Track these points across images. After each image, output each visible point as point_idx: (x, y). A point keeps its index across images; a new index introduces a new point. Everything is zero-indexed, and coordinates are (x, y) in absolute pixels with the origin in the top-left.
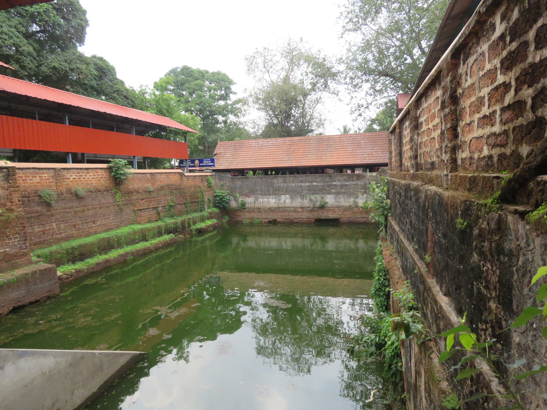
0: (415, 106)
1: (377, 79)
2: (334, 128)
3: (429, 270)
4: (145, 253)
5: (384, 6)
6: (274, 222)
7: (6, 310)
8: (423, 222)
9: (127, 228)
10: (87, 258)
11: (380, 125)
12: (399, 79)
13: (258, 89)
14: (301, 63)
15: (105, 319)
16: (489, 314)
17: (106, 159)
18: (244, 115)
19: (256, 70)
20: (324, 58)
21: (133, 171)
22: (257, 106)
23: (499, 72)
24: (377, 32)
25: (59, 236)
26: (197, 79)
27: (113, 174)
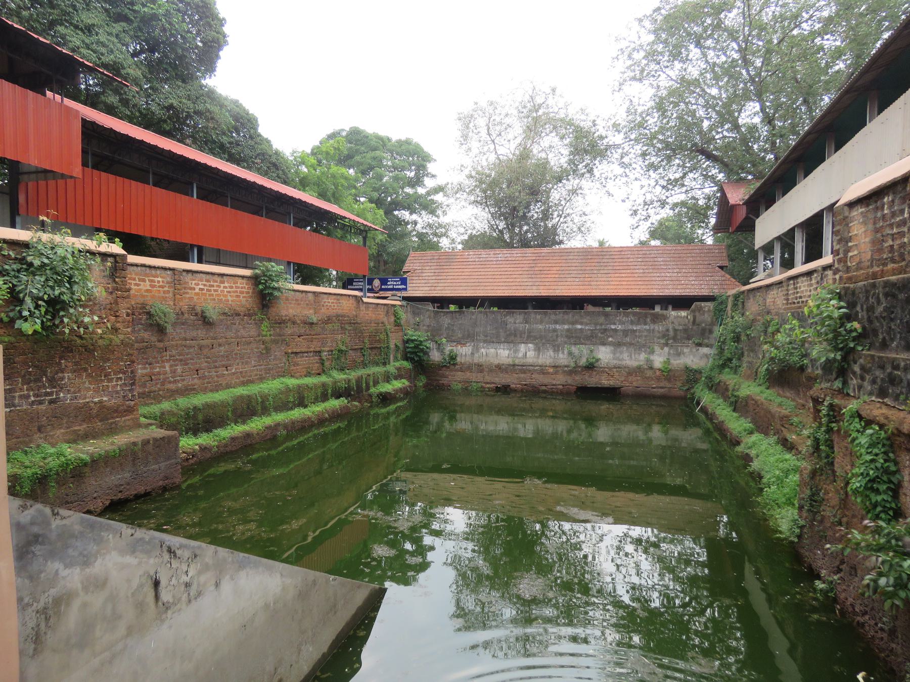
4: (304, 426)
6: (505, 390)
10: (216, 428)
20: (594, 121)
25: (172, 386)
26: (375, 149)
27: (261, 287)
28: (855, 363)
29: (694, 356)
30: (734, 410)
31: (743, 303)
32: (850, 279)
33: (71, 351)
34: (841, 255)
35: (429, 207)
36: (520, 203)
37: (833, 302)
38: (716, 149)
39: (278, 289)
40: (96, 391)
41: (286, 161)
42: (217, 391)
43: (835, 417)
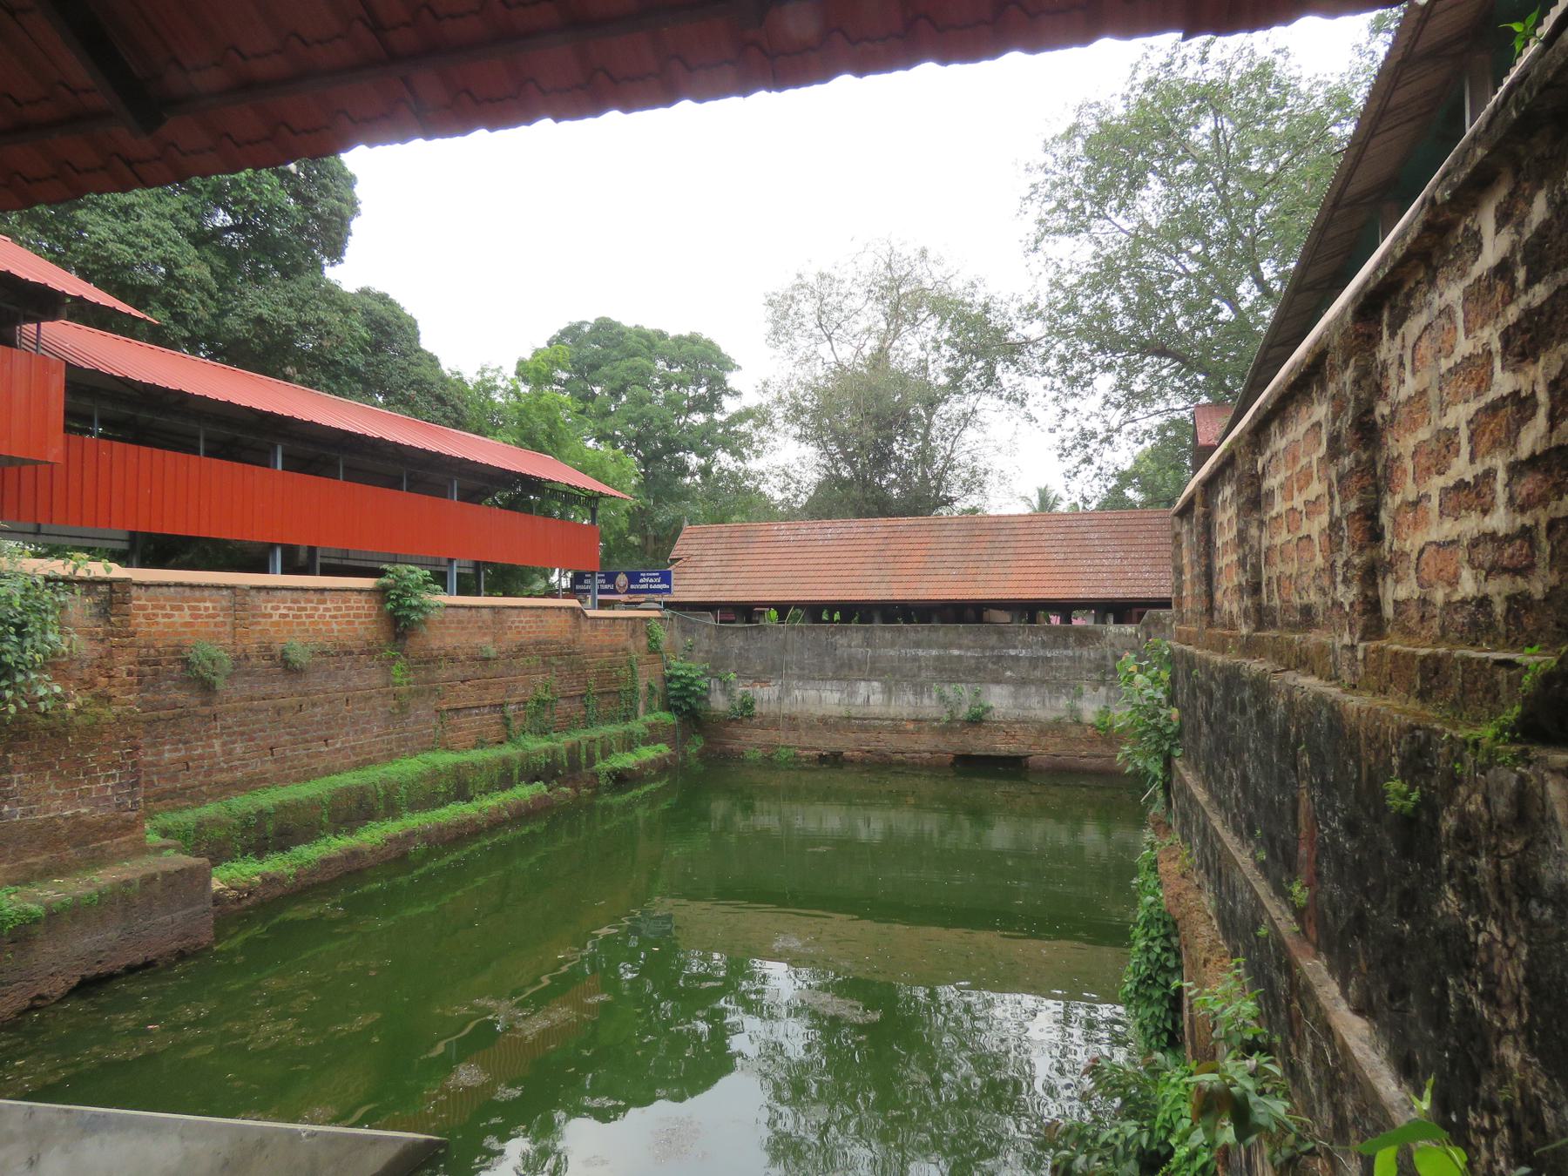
0: (1249, 444)
1: (1136, 361)
2: (1012, 494)
3: (1304, 931)
5: (1154, 170)
6: (834, 760)
7: (60, 986)
8: (1282, 783)
9: (414, 760)
10: (297, 844)
11: (1143, 490)
12: (1199, 365)
13: (800, 383)
14: (921, 316)
15: (332, 1029)
16: (1503, 1081)
17: (375, 565)
18: (758, 454)
19: (798, 332)
20: (986, 305)
21: (444, 599)
22: (796, 430)
23: (1498, 363)
24: (1136, 236)
25: (225, 777)
27: (389, 606)
33: (26, 738)
40: (69, 798)
42: (308, 780)
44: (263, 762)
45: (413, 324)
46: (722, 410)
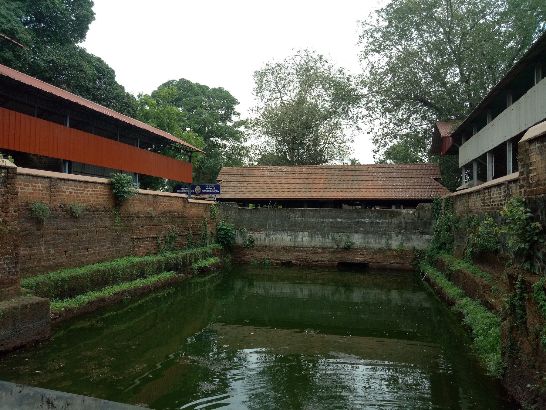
4: (144, 292)
6: (288, 264)
9: (123, 260)
10: (78, 295)
18: (246, 140)
20: (348, 79)
25: (45, 264)
28: (539, 251)
29: (419, 241)
30: (449, 280)
31: (453, 204)
32: (532, 192)
34: (525, 176)
35: (235, 135)
36: (299, 132)
37: (522, 208)
38: (432, 99)
39: (128, 193)
41: (134, 101)
43: (526, 289)
44: (62, 258)
45: (113, 72)
46: (231, 121)
